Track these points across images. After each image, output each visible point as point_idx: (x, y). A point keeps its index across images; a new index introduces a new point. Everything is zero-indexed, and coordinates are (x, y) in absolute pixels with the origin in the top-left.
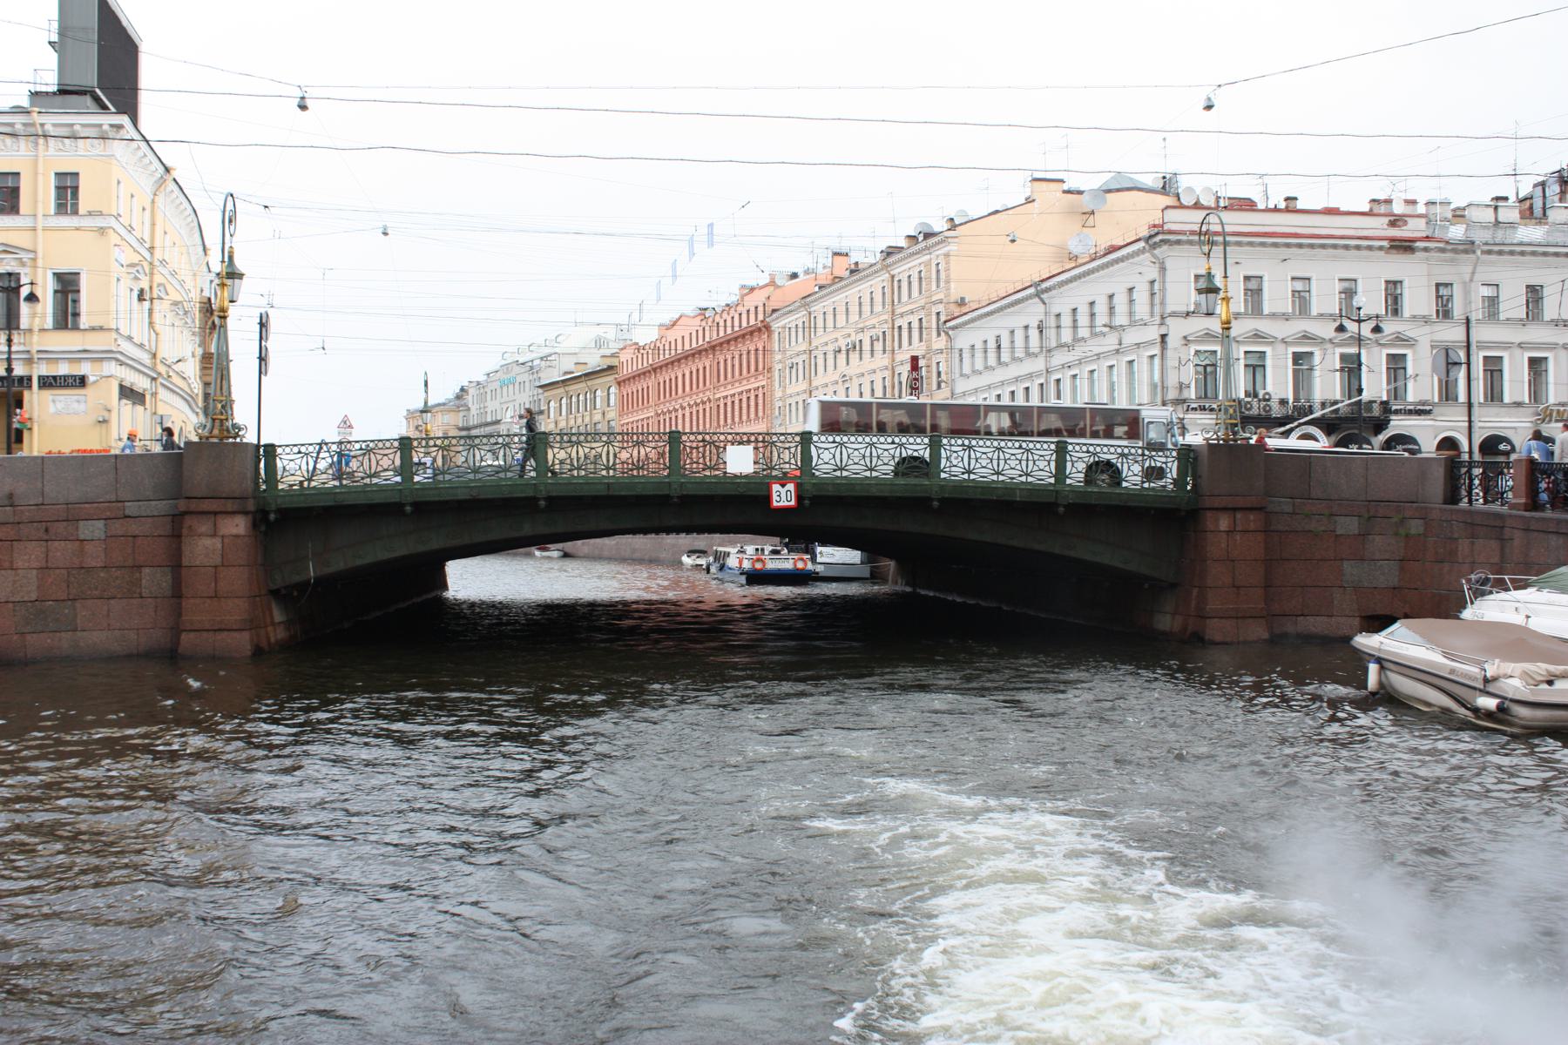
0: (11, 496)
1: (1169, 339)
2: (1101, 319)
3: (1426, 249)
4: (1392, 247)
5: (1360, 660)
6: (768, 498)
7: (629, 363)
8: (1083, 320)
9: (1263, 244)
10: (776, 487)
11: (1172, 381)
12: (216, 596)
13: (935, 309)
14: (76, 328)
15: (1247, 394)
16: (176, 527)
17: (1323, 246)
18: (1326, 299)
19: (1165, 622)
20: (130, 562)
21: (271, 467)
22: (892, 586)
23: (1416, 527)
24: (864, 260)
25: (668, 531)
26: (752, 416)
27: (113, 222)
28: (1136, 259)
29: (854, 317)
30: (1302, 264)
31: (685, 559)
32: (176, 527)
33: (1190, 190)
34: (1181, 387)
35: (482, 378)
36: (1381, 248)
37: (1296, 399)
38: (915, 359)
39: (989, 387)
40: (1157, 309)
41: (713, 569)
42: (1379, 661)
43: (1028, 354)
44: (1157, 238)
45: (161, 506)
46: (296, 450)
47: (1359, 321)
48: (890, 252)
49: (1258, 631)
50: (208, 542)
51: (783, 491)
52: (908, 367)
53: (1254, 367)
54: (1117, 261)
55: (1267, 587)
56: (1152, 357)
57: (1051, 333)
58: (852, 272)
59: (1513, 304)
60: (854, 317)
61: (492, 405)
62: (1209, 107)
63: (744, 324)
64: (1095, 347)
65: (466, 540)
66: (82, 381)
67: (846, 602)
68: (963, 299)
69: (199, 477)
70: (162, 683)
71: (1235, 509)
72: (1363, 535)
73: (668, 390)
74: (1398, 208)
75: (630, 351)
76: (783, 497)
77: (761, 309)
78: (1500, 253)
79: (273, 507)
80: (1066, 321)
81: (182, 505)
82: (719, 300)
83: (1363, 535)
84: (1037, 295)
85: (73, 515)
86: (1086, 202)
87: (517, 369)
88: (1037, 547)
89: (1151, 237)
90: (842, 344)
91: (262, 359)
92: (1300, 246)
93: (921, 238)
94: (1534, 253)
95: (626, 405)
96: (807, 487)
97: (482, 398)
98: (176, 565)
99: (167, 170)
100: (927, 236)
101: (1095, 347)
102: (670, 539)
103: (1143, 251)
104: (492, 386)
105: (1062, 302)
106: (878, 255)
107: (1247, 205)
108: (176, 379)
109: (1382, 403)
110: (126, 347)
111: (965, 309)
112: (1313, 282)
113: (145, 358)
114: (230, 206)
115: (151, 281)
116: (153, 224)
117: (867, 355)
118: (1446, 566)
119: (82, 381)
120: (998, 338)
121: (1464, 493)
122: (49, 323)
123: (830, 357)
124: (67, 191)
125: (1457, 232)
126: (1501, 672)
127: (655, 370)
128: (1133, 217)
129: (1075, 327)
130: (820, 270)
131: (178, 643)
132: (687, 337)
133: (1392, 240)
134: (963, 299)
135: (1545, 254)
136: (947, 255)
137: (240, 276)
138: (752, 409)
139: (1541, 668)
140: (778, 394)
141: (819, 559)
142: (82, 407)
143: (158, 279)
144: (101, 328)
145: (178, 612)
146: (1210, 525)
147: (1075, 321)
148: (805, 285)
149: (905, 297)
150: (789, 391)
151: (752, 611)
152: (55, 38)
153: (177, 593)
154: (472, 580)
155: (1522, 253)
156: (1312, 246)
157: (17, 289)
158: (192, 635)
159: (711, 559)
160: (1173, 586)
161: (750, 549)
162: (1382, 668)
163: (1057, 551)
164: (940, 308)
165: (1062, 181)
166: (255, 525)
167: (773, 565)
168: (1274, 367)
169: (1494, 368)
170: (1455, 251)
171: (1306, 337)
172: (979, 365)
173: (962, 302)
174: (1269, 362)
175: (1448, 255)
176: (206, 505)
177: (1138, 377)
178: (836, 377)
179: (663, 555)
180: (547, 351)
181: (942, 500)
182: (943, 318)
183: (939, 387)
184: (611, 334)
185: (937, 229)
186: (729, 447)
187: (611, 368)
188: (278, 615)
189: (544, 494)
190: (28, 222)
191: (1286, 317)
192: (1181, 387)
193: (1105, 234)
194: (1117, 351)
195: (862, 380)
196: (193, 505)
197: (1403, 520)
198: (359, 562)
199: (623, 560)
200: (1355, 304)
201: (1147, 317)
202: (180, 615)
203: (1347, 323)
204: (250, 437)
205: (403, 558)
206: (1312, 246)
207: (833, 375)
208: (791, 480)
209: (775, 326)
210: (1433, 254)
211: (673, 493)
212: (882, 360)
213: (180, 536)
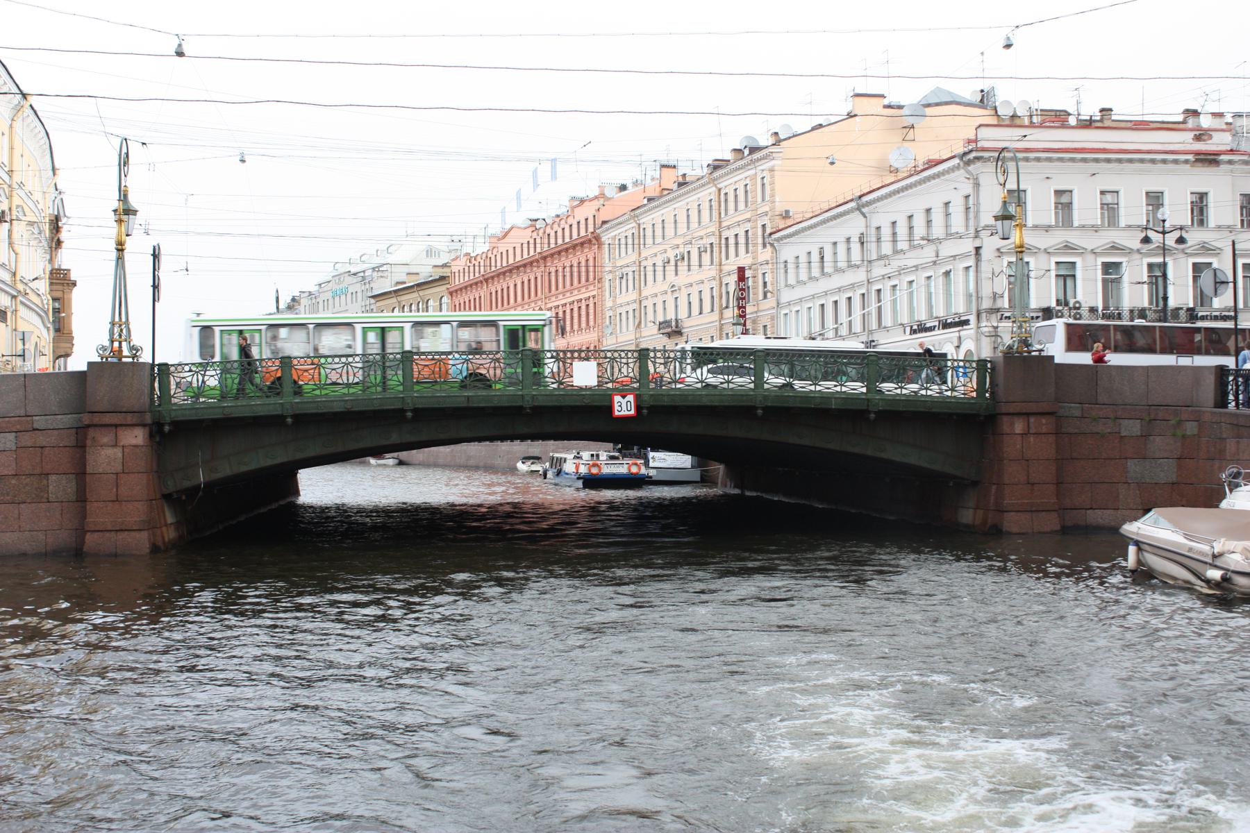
1: (982, 251)
2: (920, 230)
3: (1230, 162)
4: (1197, 160)
5: (1124, 542)
6: (610, 408)
7: (461, 273)
8: (902, 231)
9: (1073, 160)
11: (986, 291)
16: (81, 439)
17: (1131, 161)
18: (1133, 211)
19: (967, 516)
20: (38, 471)
21: (165, 386)
23: (1191, 428)
24: (692, 174)
26: (584, 325)
28: (952, 175)
30: (1110, 178)
31: (520, 465)
32: (81, 439)
33: (1007, 103)
34: (995, 296)
35: (314, 289)
36: (1186, 162)
37: (1106, 307)
38: (741, 270)
39: (813, 297)
40: (971, 222)
41: (550, 475)
43: (851, 266)
44: (971, 156)
45: (67, 420)
46: (187, 368)
47: (1164, 233)
48: (717, 166)
49: (1050, 522)
50: (110, 452)
51: (624, 402)
52: (735, 277)
53: (1065, 277)
54: (938, 176)
55: (1058, 483)
56: (967, 268)
57: (873, 246)
58: (680, 185)
62: (1008, 46)
63: (575, 236)
64: (911, 260)
65: (340, 449)
67: (686, 502)
68: (787, 212)
69: (101, 394)
70: (74, 575)
71: (1028, 414)
72: (1145, 436)
74: (1205, 122)
75: (463, 260)
76: (624, 407)
77: (591, 222)
79: (168, 420)
81: (86, 419)
82: (548, 212)
83: (1145, 436)
84: (858, 209)
88: (850, 449)
89: (965, 154)
90: (671, 254)
91: (156, 287)
92: (1108, 161)
93: (747, 152)
96: (646, 398)
98: (81, 473)
100: (753, 150)
101: (911, 260)
102: (505, 446)
103: (958, 167)
104: (323, 297)
105: (882, 216)
106: (706, 170)
107: (1058, 118)
108: (32, 297)
109: (1189, 309)
111: (789, 222)
112: (1121, 194)
114: (124, 150)
115: (11, 203)
116: (12, 148)
117: (695, 267)
118: (1217, 463)
120: (821, 250)
121: (1231, 397)
123: (659, 269)
126: (1226, 548)
128: (947, 134)
129: (894, 241)
130: (649, 182)
131: (83, 542)
132: (516, 248)
133: (1197, 153)
134: (787, 212)
136: (772, 170)
137: (135, 212)
138: (584, 319)
140: (609, 304)
141: (651, 464)
145: (83, 515)
146: (1006, 428)
147: (894, 234)
148: (635, 196)
150: (619, 301)
153: (82, 497)
154: (320, 487)
156: (1120, 161)
158: (96, 535)
159: (548, 464)
160: (975, 484)
161: (586, 455)
162: (1140, 549)
163: (869, 452)
164: (766, 220)
165: (883, 96)
166: (151, 436)
167: (609, 469)
168: (1084, 280)
171: (1115, 248)
172: (803, 276)
173: (786, 215)
174: (1079, 274)
176: (107, 419)
178: (665, 287)
179: (498, 462)
180: (379, 261)
182: (768, 231)
183: (765, 297)
184: (441, 244)
185: (762, 143)
186: (576, 364)
187: (442, 278)
188: (170, 519)
189: (411, 406)
191: (1096, 229)
192: (995, 296)
193: (923, 150)
194: (935, 263)
195: (690, 290)
196: (97, 419)
197: (1180, 423)
198: (244, 469)
199: (445, 466)
200: (1160, 216)
201: (962, 230)
202: (85, 517)
203: (1151, 234)
204: (146, 357)
205: (282, 464)
206: (1120, 161)
207: (662, 286)
208: (632, 391)
209: (606, 238)
210: (1237, 166)
211: (526, 405)
212: (709, 272)
213: (84, 447)
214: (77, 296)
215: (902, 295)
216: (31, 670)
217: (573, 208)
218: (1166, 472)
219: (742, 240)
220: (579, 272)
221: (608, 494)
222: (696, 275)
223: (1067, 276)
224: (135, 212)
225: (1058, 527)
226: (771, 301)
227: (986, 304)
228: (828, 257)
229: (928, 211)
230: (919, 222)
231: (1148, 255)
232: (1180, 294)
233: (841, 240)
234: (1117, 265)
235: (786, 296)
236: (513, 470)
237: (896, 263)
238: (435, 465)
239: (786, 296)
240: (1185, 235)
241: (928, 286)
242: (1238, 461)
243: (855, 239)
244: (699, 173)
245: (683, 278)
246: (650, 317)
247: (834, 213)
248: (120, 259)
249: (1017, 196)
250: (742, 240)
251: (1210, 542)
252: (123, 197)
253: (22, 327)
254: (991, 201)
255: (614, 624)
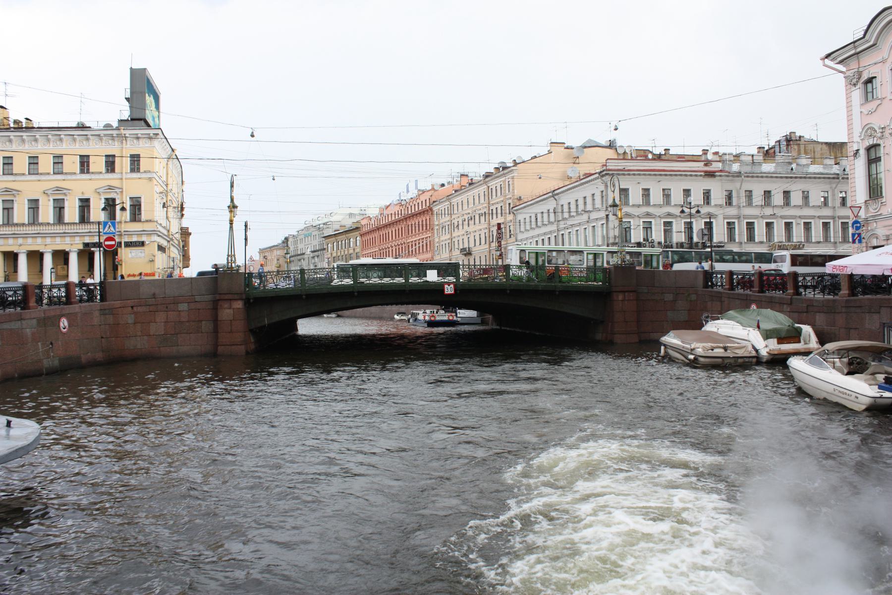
0: (154, 294)
2: (581, 207)
5: (661, 344)
6: (443, 290)
9: (650, 175)
10: (446, 286)
11: (611, 234)
12: (231, 332)
13: (508, 202)
14: (140, 221)
15: (644, 240)
16: (215, 305)
17: (676, 175)
18: (677, 197)
19: (599, 336)
22: (492, 326)
23: (694, 297)
24: (476, 179)
25: (387, 305)
27: (155, 176)
29: (471, 205)
31: (396, 316)
32: (215, 305)
37: (665, 242)
41: (411, 321)
42: (665, 345)
43: (550, 223)
45: (209, 297)
48: (487, 176)
49: (634, 339)
50: (228, 311)
52: (496, 228)
54: (589, 181)
59: (758, 199)
60: (471, 205)
61: (300, 246)
62: (616, 129)
66: (142, 244)
67: (475, 333)
73: (385, 238)
74: (710, 157)
78: (752, 177)
80: (566, 209)
81: (218, 297)
85: (176, 301)
86: (575, 153)
87: (313, 229)
90: (466, 217)
91: (246, 239)
92: (666, 175)
94: (767, 177)
95: (364, 245)
97: (296, 243)
98: (215, 320)
99: (173, 150)
100: (504, 168)
102: (388, 308)
105: (564, 200)
110: (160, 229)
113: (165, 232)
119: (142, 244)
122: (128, 219)
124: (135, 160)
125: (735, 167)
127: (378, 229)
128: (596, 159)
129: (570, 212)
133: (705, 172)
135: (772, 177)
137: (236, 207)
139: (709, 345)
140: (437, 240)
142: (143, 255)
143: (169, 198)
144: (150, 221)
145: (217, 338)
149: (494, 197)
150: (442, 239)
151: (426, 337)
152: (128, 96)
153: (216, 330)
154: (307, 327)
155: (762, 177)
156: (671, 175)
157: (114, 205)
164: (510, 201)
166: (245, 304)
169: (750, 226)
170: (733, 176)
171: (669, 215)
172: (528, 227)
173: (520, 199)
175: (730, 178)
176: (226, 297)
177: (584, 240)
179: (385, 315)
180: (325, 221)
181: (511, 290)
185: (508, 165)
187: (357, 228)
188: (252, 340)
190: (119, 176)
196: (223, 297)
197: (689, 295)
198: (284, 318)
203: (685, 209)
206: (671, 175)
209: (435, 209)
212: (484, 225)
214: (192, 239)
215: (574, 237)
216: (827, 112)
217: (419, 195)
218: (683, 316)
219: (499, 211)
221: (441, 330)
222: (477, 227)
223: (648, 228)
224: (236, 207)
225: (637, 340)
226: (513, 239)
227: (611, 241)
228: (539, 219)
229: (585, 198)
230: (581, 202)
231: (684, 218)
232: (719, 234)
233: (545, 211)
234: (670, 223)
235: (520, 237)
236: (393, 319)
237: (570, 222)
238: (355, 317)
239: (520, 237)
240: (700, 209)
241: (585, 233)
242: (707, 311)
243: (552, 211)
244: (480, 179)
245: (472, 228)
246: (456, 246)
247: (541, 199)
248: (231, 227)
249: (624, 192)
250: (499, 211)
251: (690, 344)
252: (232, 200)
253: (172, 255)
254: (614, 196)
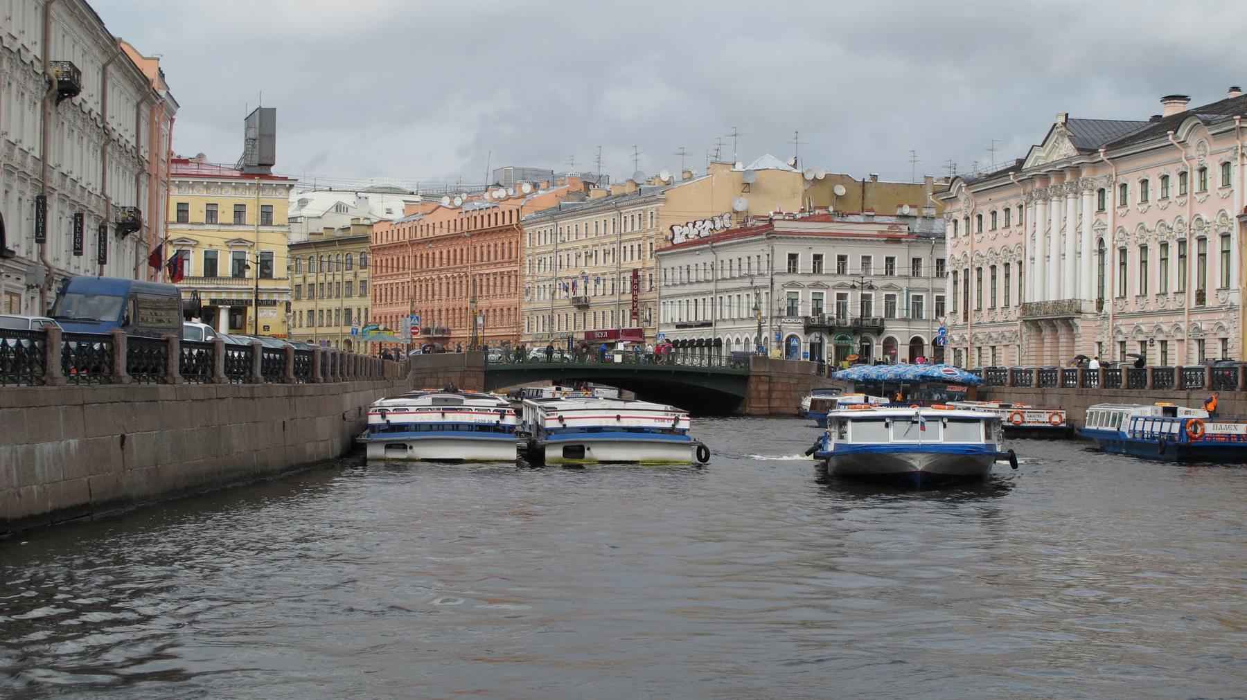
11: (775, 307)
149: (629, 229)
220: (496, 252)
227: (776, 314)
239: (664, 292)
255: (148, 590)
